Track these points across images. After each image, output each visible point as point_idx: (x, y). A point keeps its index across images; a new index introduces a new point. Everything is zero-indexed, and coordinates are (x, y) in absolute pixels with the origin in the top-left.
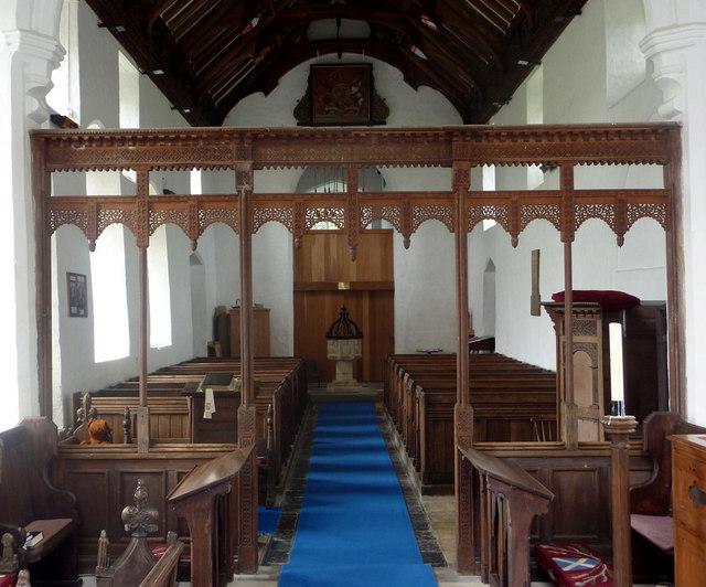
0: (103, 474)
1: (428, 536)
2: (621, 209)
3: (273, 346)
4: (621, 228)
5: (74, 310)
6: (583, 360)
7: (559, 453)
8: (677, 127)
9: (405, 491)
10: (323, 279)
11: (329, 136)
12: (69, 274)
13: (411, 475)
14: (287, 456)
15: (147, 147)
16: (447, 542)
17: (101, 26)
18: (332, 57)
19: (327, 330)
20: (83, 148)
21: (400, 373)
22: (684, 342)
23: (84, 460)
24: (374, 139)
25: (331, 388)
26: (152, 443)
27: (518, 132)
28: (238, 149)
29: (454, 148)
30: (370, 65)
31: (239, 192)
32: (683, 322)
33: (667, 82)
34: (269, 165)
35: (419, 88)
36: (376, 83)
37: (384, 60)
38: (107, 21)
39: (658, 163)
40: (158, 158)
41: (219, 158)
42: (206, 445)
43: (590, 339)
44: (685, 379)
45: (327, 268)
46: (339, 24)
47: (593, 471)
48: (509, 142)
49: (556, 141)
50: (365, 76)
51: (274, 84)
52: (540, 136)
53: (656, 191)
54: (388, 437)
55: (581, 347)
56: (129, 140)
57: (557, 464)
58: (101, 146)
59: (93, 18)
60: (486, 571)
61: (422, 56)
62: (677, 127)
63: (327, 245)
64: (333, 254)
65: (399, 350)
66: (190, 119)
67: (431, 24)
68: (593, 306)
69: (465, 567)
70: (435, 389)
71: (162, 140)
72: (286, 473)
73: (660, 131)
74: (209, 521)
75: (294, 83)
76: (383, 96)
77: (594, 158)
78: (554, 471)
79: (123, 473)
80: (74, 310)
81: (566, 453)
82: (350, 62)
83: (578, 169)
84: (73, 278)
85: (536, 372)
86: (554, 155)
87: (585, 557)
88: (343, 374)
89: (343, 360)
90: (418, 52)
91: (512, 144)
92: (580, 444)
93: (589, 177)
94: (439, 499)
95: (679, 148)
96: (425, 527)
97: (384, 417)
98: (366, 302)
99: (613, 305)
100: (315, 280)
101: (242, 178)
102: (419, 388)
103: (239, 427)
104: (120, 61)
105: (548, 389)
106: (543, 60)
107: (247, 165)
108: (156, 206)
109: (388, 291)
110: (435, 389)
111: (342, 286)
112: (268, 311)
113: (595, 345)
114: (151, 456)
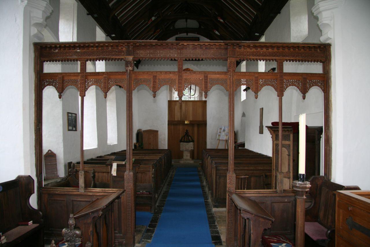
3: (159, 144)
4: (304, 91)
5: (71, 128)
6: (285, 152)
8: (329, 45)
10: (179, 119)
12: (68, 113)
13: (210, 198)
17: (88, 14)
20: (57, 51)
21: (207, 156)
22: (332, 144)
23: (58, 194)
25: (182, 162)
29: (228, 51)
30: (199, 38)
31: (127, 70)
32: (331, 134)
33: (327, 25)
37: (205, 37)
38: (91, 13)
39: (321, 62)
42: (110, 189)
45: (181, 115)
46: (186, 21)
53: (319, 74)
54: (202, 182)
56: (77, 47)
58: (65, 50)
59: (85, 11)
61: (219, 34)
62: (329, 45)
65: (209, 146)
67: (222, 20)
68: (289, 128)
71: (92, 47)
77: (292, 58)
78: (272, 203)
79: (73, 201)
81: (277, 195)
84: (70, 115)
85: (270, 157)
87: (284, 242)
88: (187, 156)
89: (186, 150)
90: (217, 32)
91: (255, 50)
93: (289, 67)
97: (201, 173)
98: (196, 129)
100: (176, 119)
104: (97, 30)
108: (89, 77)
113: (289, 145)
114: (86, 193)
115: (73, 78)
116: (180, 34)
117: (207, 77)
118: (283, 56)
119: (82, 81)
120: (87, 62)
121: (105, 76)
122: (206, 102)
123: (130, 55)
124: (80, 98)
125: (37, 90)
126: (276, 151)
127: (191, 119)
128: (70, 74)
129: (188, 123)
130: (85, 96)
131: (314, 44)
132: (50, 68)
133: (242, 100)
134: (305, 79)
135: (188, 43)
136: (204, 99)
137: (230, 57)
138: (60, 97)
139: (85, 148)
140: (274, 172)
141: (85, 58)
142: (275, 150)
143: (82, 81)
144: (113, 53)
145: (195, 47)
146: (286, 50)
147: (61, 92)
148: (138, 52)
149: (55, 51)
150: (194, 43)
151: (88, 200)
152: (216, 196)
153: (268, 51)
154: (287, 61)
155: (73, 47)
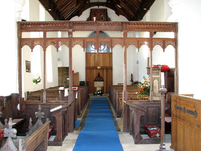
1: (117, 126)
2: (164, 43)
4: (164, 47)
7: (148, 103)
10: (93, 66)
15: (46, 26)
16: (121, 127)
18: (96, 7)
19: (94, 79)
20: (30, 26)
30: (107, 9)
34: (77, 30)
35: (120, 16)
36: (108, 14)
41: (64, 29)
44: (178, 84)
47: (156, 107)
48: (137, 26)
49: (148, 26)
50: (105, 11)
51: (81, 14)
52: (142, 24)
54: (109, 106)
55: (155, 78)
56: (41, 24)
57: (148, 105)
60: (131, 132)
63: (95, 56)
64: (96, 59)
66: (55, 19)
69: (125, 131)
71: (50, 24)
73: (173, 24)
74: (61, 118)
75: (86, 15)
76: (110, 17)
80: (27, 70)
81: (150, 103)
82: (101, 8)
84: (27, 62)
86: (148, 29)
90: (119, 6)
92: (154, 101)
94: (120, 119)
95: (177, 28)
98: (105, 70)
99: (165, 69)
100: (91, 66)
101: (70, 33)
106: (150, 8)
107: (71, 30)
109: (111, 68)
113: (159, 78)
114: (47, 104)
116: (93, 6)
117: (112, 40)
122: (112, 53)
123: (70, 29)
127: (102, 66)
129: (100, 68)
130: (46, 51)
131: (169, 23)
132: (25, 35)
136: (110, 51)
144: (62, 28)
145: (105, 25)
146: (154, 26)
152: (118, 111)
155: (39, 24)
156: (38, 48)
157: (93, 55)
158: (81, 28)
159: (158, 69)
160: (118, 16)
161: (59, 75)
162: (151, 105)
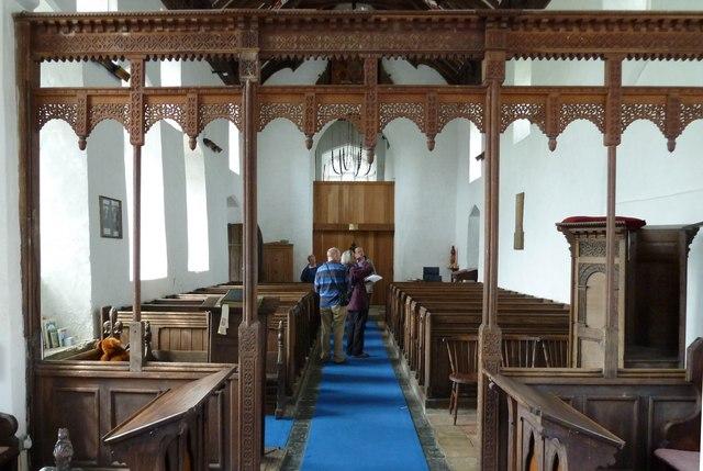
0: (94, 393)
5: (107, 231)
7: (596, 381)
9: (409, 402)
11: (347, 21)
12: (102, 198)
14: (303, 367)
20: (73, 34)
24: (397, 26)
26: (148, 359)
27: (561, 18)
28: (244, 35)
29: (487, 35)
40: (155, 45)
43: (601, 260)
45: (340, 214)
48: (549, 31)
55: (597, 268)
58: (92, 32)
63: (341, 192)
65: (396, 280)
70: (437, 310)
72: (299, 385)
76: (388, 73)
81: (603, 381)
83: (626, 64)
84: (105, 202)
91: (552, 33)
93: (639, 73)
96: (431, 441)
102: (423, 310)
103: (240, 347)
105: (477, 311)
108: (153, 100)
109: (389, 232)
110: (437, 310)
111: (351, 228)
112: (292, 245)
114: (145, 375)
115: (114, 101)
118: (623, 45)
119: (136, 109)
120: (147, 63)
121: (190, 96)
124: (129, 150)
125: (26, 113)
126: (579, 281)
128: (106, 93)
130: (143, 144)
132: (54, 75)
133: (471, 180)
134: (677, 101)
135: (390, 16)
137: (491, 50)
138: (83, 146)
139: (142, 278)
140: (576, 327)
141: (142, 53)
142: (577, 279)
143: (136, 109)
147: (85, 131)
148: (271, 38)
149: (67, 36)
150: (404, 16)
151: (151, 391)
153: (584, 34)
154: (630, 58)
156: (582, 134)
157: (336, 189)
158: (298, 42)
159: (595, 232)
160: (416, 67)
161: (230, 248)
162: (611, 393)
